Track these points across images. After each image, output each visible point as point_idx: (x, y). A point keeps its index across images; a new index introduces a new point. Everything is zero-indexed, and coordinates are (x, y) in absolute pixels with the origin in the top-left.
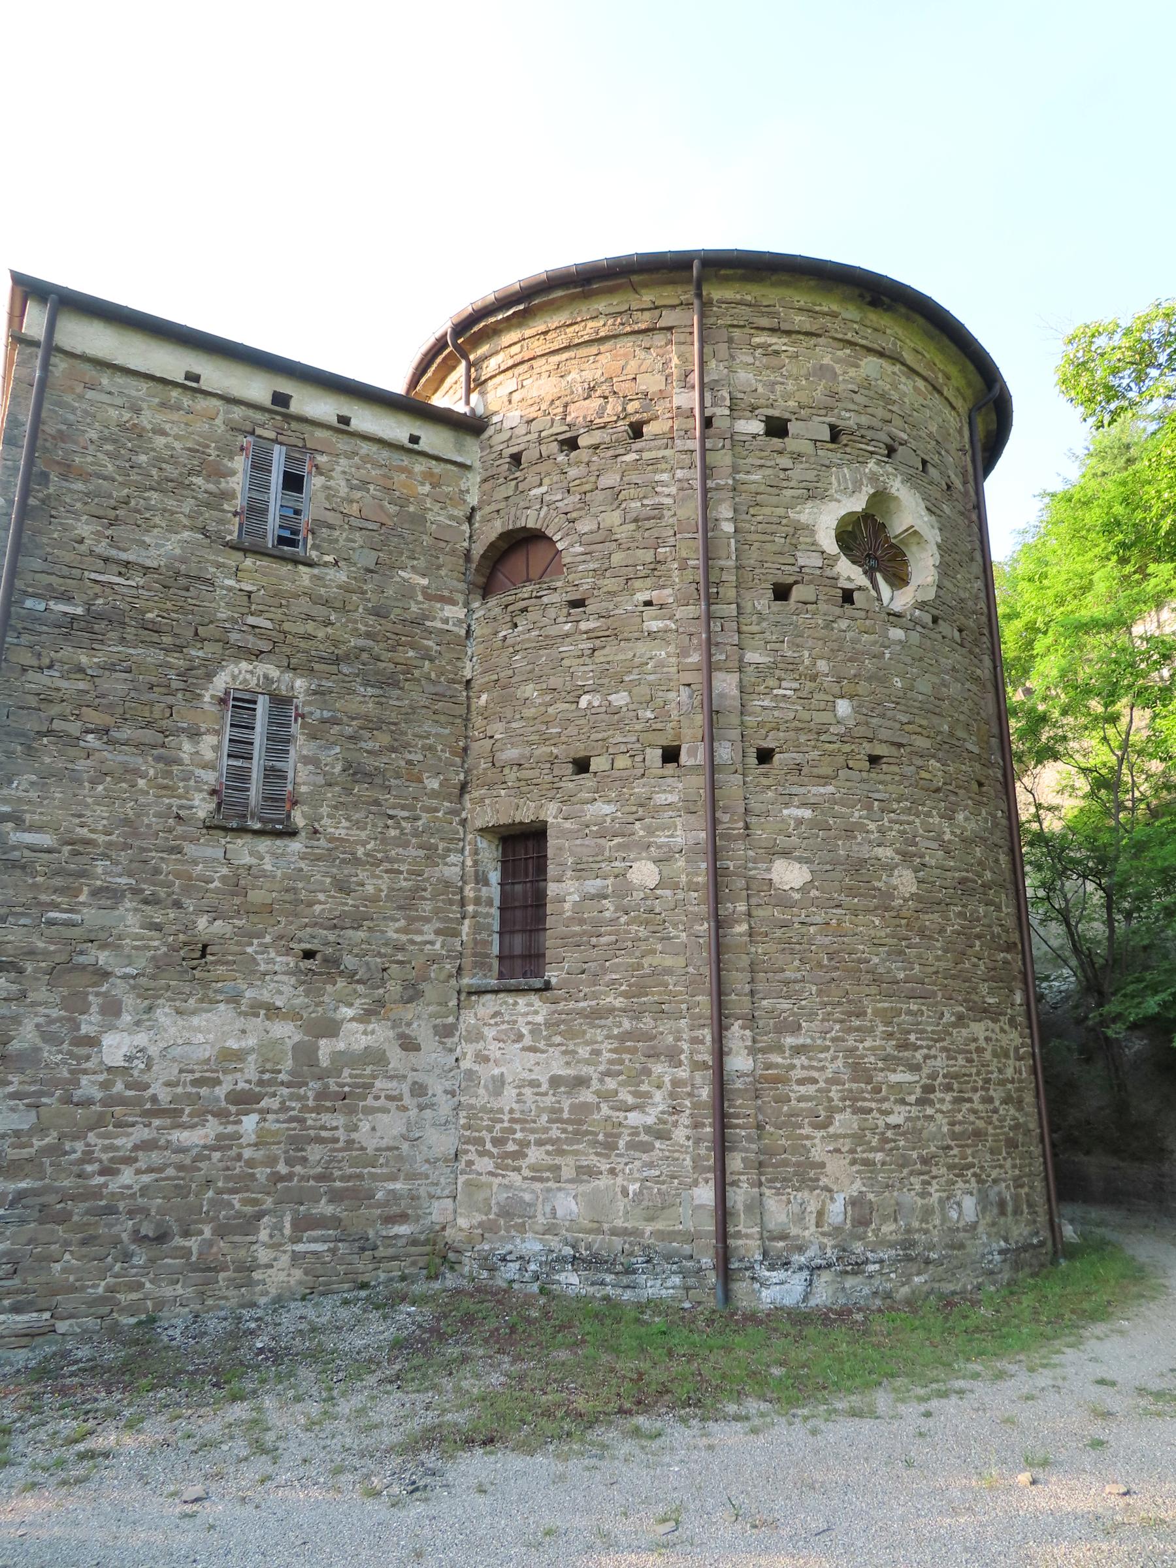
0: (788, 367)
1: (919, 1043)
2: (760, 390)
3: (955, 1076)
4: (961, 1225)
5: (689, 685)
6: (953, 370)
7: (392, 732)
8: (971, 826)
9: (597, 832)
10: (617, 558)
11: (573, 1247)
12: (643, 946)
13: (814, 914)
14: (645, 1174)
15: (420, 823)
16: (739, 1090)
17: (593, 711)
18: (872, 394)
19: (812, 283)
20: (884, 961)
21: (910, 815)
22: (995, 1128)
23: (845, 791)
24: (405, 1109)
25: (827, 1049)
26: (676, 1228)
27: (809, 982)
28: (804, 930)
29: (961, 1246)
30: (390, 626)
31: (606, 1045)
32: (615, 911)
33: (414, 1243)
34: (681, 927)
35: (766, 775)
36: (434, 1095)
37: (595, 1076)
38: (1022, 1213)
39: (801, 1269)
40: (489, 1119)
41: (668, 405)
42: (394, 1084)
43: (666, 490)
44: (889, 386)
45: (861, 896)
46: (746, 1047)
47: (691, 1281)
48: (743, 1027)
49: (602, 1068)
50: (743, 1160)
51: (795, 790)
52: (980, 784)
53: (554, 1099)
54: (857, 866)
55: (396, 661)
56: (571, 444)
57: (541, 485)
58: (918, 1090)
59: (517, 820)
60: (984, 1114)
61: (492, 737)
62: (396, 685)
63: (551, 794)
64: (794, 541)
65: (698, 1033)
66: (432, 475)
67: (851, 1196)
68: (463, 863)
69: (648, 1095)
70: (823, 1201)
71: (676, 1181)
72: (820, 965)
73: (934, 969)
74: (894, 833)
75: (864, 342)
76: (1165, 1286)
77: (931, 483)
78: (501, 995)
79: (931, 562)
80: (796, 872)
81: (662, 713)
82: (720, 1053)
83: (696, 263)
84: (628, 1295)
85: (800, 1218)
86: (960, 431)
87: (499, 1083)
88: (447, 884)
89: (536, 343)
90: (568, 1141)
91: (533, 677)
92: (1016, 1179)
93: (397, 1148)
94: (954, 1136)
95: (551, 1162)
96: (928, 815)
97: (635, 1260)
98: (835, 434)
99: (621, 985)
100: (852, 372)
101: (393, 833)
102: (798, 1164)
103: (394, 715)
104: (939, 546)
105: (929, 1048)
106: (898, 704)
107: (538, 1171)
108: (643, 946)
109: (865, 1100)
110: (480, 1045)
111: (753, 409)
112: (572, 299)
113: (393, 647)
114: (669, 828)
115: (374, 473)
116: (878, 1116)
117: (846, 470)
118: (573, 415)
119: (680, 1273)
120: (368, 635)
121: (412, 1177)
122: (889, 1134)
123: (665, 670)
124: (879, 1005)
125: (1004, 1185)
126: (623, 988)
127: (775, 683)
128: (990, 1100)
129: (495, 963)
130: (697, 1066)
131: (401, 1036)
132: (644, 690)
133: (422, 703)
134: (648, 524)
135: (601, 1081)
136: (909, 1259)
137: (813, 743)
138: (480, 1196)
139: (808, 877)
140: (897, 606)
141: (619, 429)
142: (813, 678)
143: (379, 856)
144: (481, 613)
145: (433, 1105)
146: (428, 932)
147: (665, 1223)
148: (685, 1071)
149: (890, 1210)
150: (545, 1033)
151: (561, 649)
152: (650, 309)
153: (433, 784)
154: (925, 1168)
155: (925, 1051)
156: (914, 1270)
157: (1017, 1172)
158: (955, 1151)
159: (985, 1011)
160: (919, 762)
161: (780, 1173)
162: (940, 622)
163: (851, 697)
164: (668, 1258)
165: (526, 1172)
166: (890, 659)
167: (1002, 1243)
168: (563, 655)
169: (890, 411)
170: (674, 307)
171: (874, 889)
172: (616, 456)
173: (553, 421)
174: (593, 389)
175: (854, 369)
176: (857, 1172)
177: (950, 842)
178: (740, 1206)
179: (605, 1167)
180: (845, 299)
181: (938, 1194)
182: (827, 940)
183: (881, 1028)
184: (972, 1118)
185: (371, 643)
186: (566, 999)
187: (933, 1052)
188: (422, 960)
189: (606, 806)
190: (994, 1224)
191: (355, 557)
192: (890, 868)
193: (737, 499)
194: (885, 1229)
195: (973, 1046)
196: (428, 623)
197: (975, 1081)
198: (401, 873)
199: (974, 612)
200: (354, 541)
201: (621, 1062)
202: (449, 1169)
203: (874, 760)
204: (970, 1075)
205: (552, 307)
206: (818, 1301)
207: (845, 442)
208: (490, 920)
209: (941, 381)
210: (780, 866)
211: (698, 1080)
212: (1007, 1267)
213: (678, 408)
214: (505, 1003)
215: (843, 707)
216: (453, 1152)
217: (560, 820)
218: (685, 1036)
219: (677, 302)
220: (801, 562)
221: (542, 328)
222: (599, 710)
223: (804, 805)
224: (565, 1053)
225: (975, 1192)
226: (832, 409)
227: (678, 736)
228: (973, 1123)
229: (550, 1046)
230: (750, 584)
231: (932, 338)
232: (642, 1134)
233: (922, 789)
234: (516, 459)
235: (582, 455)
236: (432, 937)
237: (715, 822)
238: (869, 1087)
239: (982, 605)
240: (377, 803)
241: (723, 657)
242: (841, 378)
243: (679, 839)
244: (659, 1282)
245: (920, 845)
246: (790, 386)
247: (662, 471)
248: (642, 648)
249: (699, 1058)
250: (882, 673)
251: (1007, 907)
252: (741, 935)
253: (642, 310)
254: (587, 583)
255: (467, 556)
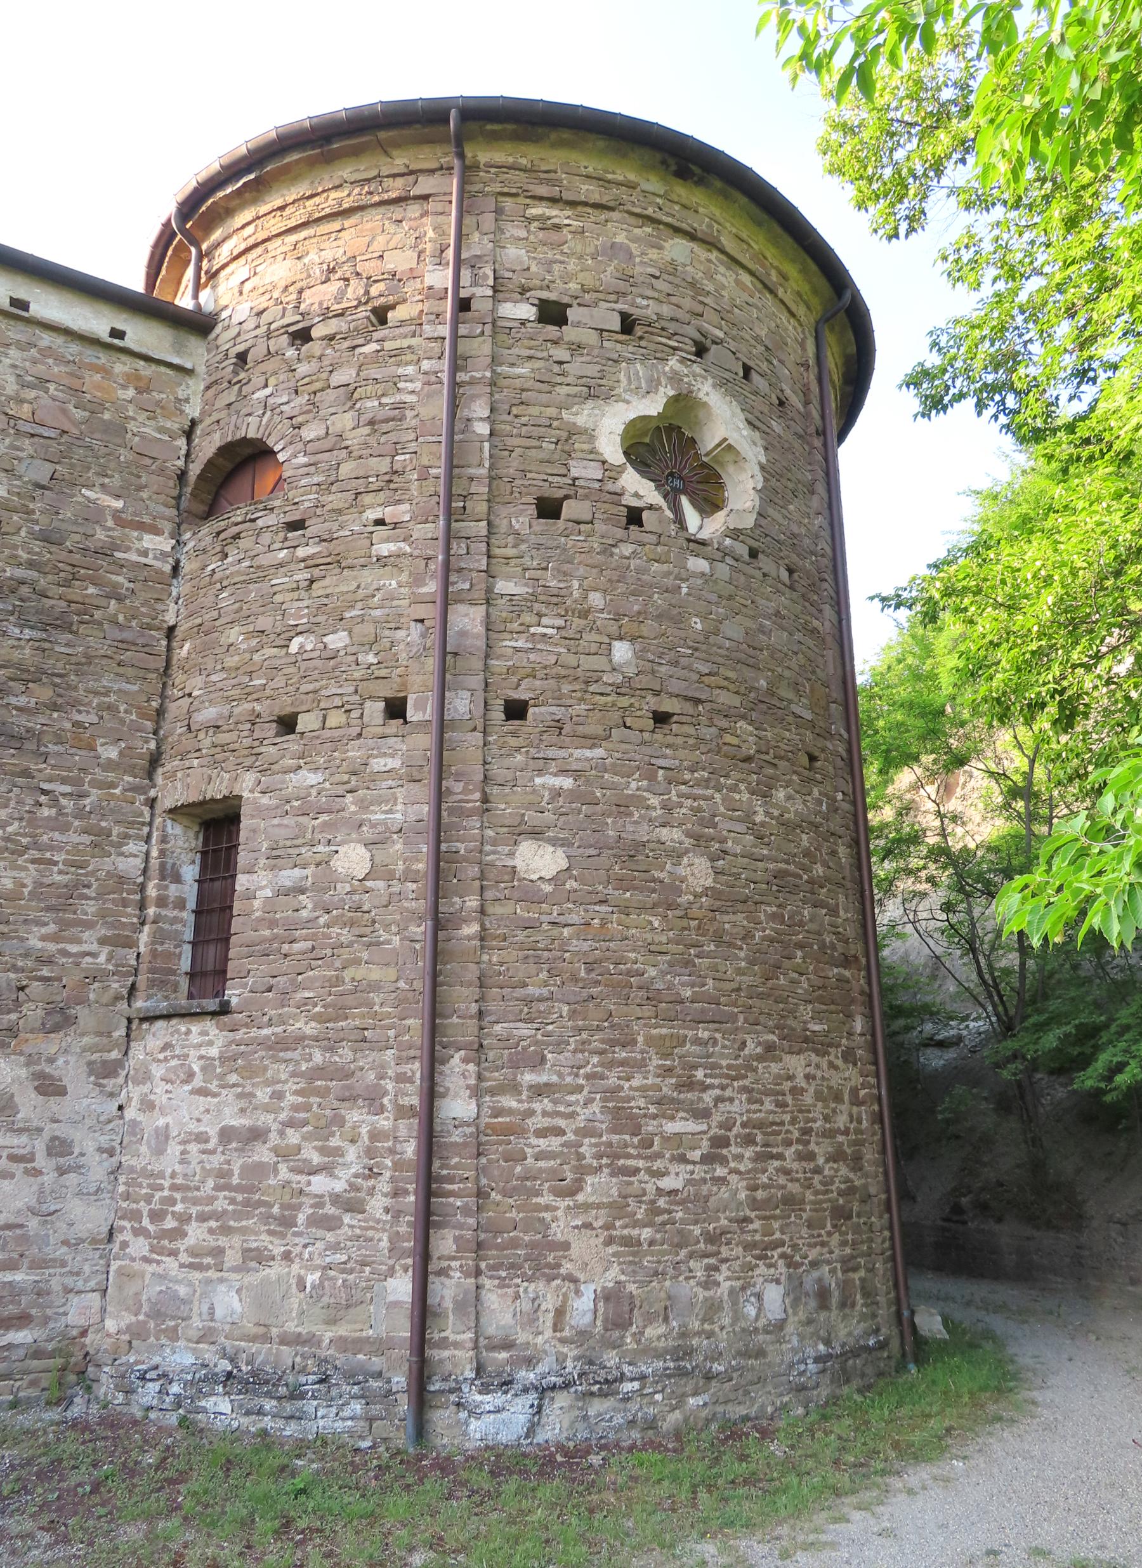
0: (571, 244)
1: (708, 1081)
2: (534, 268)
3: (760, 1125)
4: (760, 1324)
5: (422, 621)
6: (792, 271)
7: (56, 685)
8: (797, 808)
9: (299, 808)
10: (346, 469)
11: (232, 1361)
12: (346, 954)
13: (570, 911)
14: (328, 1260)
15: (87, 801)
16: (456, 1144)
17: (305, 656)
18: (677, 281)
19: (601, 144)
20: (664, 973)
21: (707, 788)
22: (816, 1193)
23: (620, 755)
24: (37, 1173)
25: (579, 1089)
26: (364, 1334)
27: (558, 1001)
28: (556, 932)
29: (760, 1353)
30: (64, 555)
31: (292, 1086)
32: (314, 910)
33: (38, 1354)
34: (394, 929)
35: (514, 734)
36: (82, 1155)
37: (275, 1127)
38: (853, 1305)
39: (525, 1390)
40: (149, 1186)
41: (419, 286)
42: (24, 1139)
43: (410, 386)
44: (700, 274)
45: (635, 889)
46: (468, 1087)
47: (377, 1409)
48: (465, 1061)
49: (283, 1116)
50: (456, 1239)
51: (552, 753)
52: (812, 758)
53: (222, 1158)
54: (632, 851)
55: (69, 597)
56: (302, 336)
57: (266, 386)
58: (705, 1144)
59: (208, 797)
60: (800, 1175)
61: (190, 695)
62: (68, 628)
63: (248, 762)
64: (567, 448)
65: (407, 1068)
66: (139, 378)
67: (604, 1288)
68: (147, 854)
69: (338, 1152)
70: (565, 1295)
71: (368, 1269)
72: (575, 979)
73: (734, 985)
74: (684, 810)
75: (669, 220)
76: (1034, 1403)
77: (756, 393)
78: (174, 1022)
79: (750, 484)
80: (548, 857)
81: (388, 659)
82: (432, 1093)
83: (453, 113)
84: (291, 1430)
85: (531, 1319)
86: (802, 345)
87: (163, 1136)
88: (121, 879)
89: (273, 221)
90: (238, 1216)
91: (241, 617)
92: (844, 1261)
93: (21, 1226)
94: (754, 1204)
95: (213, 1244)
96: (734, 789)
97: (302, 1379)
98: (628, 324)
99: (315, 1005)
100: (653, 254)
101: (46, 812)
102: (532, 1245)
103: (60, 664)
104: (762, 468)
105: (723, 1088)
106: (696, 649)
107: (196, 1256)
108: (346, 954)
109: (629, 1156)
110: (145, 1089)
111: (524, 290)
112: (312, 163)
113: (66, 580)
114: (387, 801)
115: (56, 369)
116: (647, 1178)
117: (638, 366)
118: (308, 302)
119: (362, 1397)
120: (31, 565)
121: (39, 1264)
122: (662, 1203)
123: (395, 603)
124: (654, 1032)
125: (827, 1268)
126: (317, 1009)
127: (535, 619)
128: (811, 1157)
129: (184, 983)
130: (402, 1112)
131: (40, 1076)
132: (368, 629)
133: (102, 652)
134: (385, 427)
135: (282, 1133)
136: (682, 1373)
137: (579, 694)
138: (131, 1289)
139: (564, 864)
140: (704, 535)
141: (359, 316)
142: (584, 614)
143: (25, 841)
144: (191, 545)
145: (80, 1167)
146: (89, 940)
147: (349, 1327)
148: (387, 1119)
149: (658, 1307)
150: (218, 1070)
151: (273, 582)
152: (402, 175)
153: (112, 753)
154: (711, 1248)
155: (717, 1092)
156: (689, 1389)
157: (848, 1251)
158: (756, 1225)
159: (806, 1040)
160: (724, 723)
161: (507, 1257)
162: (760, 556)
163: (633, 640)
164: (350, 1376)
165: (184, 1258)
166: (688, 594)
167: (821, 1347)
168: (276, 589)
169: (701, 302)
170: (432, 171)
171: (654, 880)
172: (354, 348)
173: (284, 309)
174: (332, 271)
175: (655, 251)
176: (614, 1255)
177: (763, 824)
178: (448, 1304)
179: (278, 1250)
180: (647, 167)
181: (728, 1284)
182: (586, 946)
183: (656, 1061)
184: (782, 1180)
185: (36, 574)
186: (246, 1025)
187: (728, 1093)
188: (77, 976)
189: (311, 775)
190: (809, 1322)
191: (21, 468)
192: (677, 855)
193: (497, 396)
194: (650, 1332)
195: (787, 1086)
196: (118, 555)
197: (788, 1131)
198: (56, 863)
199: (812, 553)
200: (22, 450)
201: (307, 1108)
202: (98, 1253)
203: (661, 718)
204: (782, 1123)
205: (287, 175)
206: (549, 1435)
207: (639, 334)
208: (179, 927)
209: (774, 279)
210: (526, 848)
211: (403, 1132)
212: (826, 1379)
213: (430, 288)
214: (177, 1031)
215: (622, 651)
216: (105, 1229)
217: (257, 794)
218: (390, 1073)
219: (435, 165)
220: (574, 472)
221: (279, 202)
222: (312, 655)
223: (563, 772)
224: (240, 1096)
225: (783, 1279)
226: (625, 294)
227: (404, 687)
228: (784, 1187)
229: (223, 1087)
230: (507, 498)
231: (759, 224)
232: (328, 1206)
233: (725, 756)
234: (242, 357)
235: (315, 347)
236: (94, 947)
237: (440, 795)
238: (636, 1140)
239: (824, 545)
240: (26, 773)
241: (467, 586)
242: (638, 260)
243: (399, 816)
244: (334, 1410)
245: (720, 826)
246: (572, 265)
247: (407, 364)
248: (368, 577)
249: (406, 1101)
250: (675, 611)
251: (846, 911)
252: (469, 938)
253: (394, 176)
254: (308, 501)
255: (182, 476)
